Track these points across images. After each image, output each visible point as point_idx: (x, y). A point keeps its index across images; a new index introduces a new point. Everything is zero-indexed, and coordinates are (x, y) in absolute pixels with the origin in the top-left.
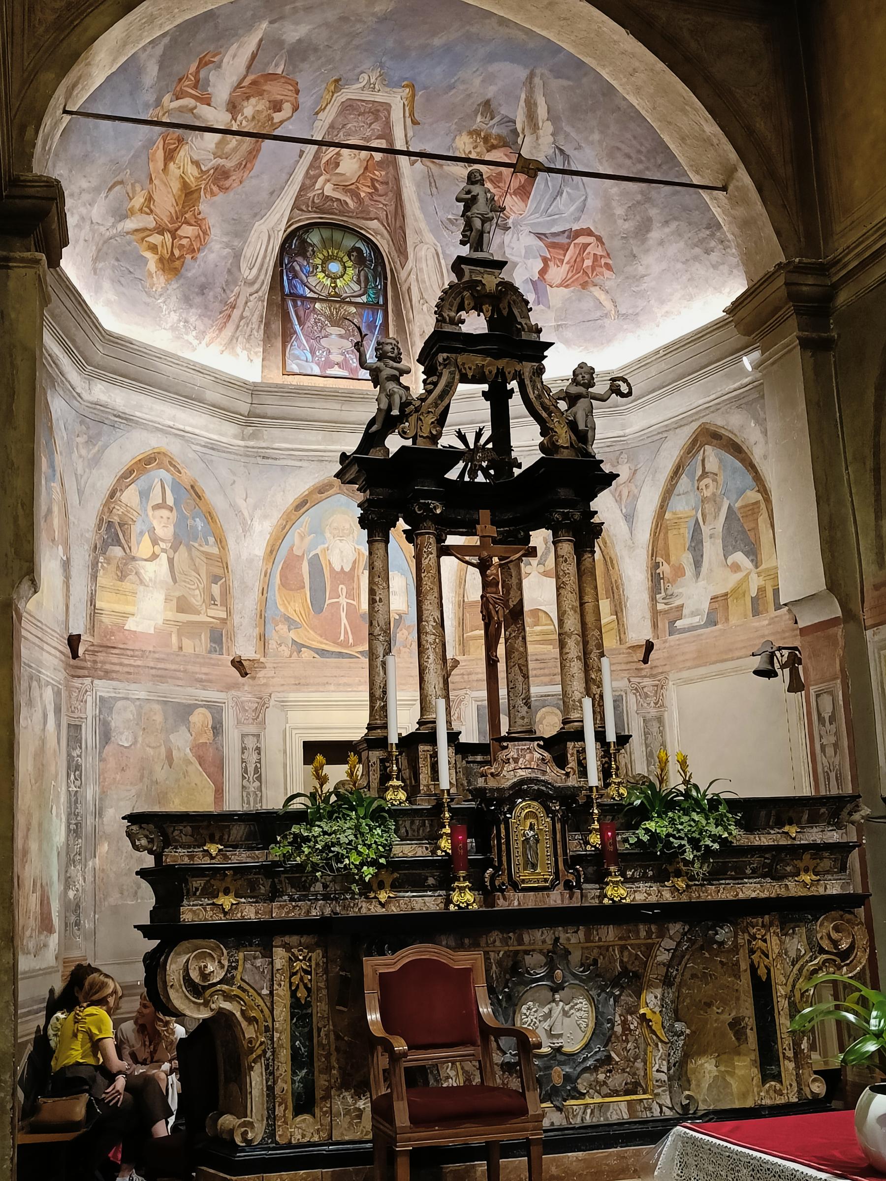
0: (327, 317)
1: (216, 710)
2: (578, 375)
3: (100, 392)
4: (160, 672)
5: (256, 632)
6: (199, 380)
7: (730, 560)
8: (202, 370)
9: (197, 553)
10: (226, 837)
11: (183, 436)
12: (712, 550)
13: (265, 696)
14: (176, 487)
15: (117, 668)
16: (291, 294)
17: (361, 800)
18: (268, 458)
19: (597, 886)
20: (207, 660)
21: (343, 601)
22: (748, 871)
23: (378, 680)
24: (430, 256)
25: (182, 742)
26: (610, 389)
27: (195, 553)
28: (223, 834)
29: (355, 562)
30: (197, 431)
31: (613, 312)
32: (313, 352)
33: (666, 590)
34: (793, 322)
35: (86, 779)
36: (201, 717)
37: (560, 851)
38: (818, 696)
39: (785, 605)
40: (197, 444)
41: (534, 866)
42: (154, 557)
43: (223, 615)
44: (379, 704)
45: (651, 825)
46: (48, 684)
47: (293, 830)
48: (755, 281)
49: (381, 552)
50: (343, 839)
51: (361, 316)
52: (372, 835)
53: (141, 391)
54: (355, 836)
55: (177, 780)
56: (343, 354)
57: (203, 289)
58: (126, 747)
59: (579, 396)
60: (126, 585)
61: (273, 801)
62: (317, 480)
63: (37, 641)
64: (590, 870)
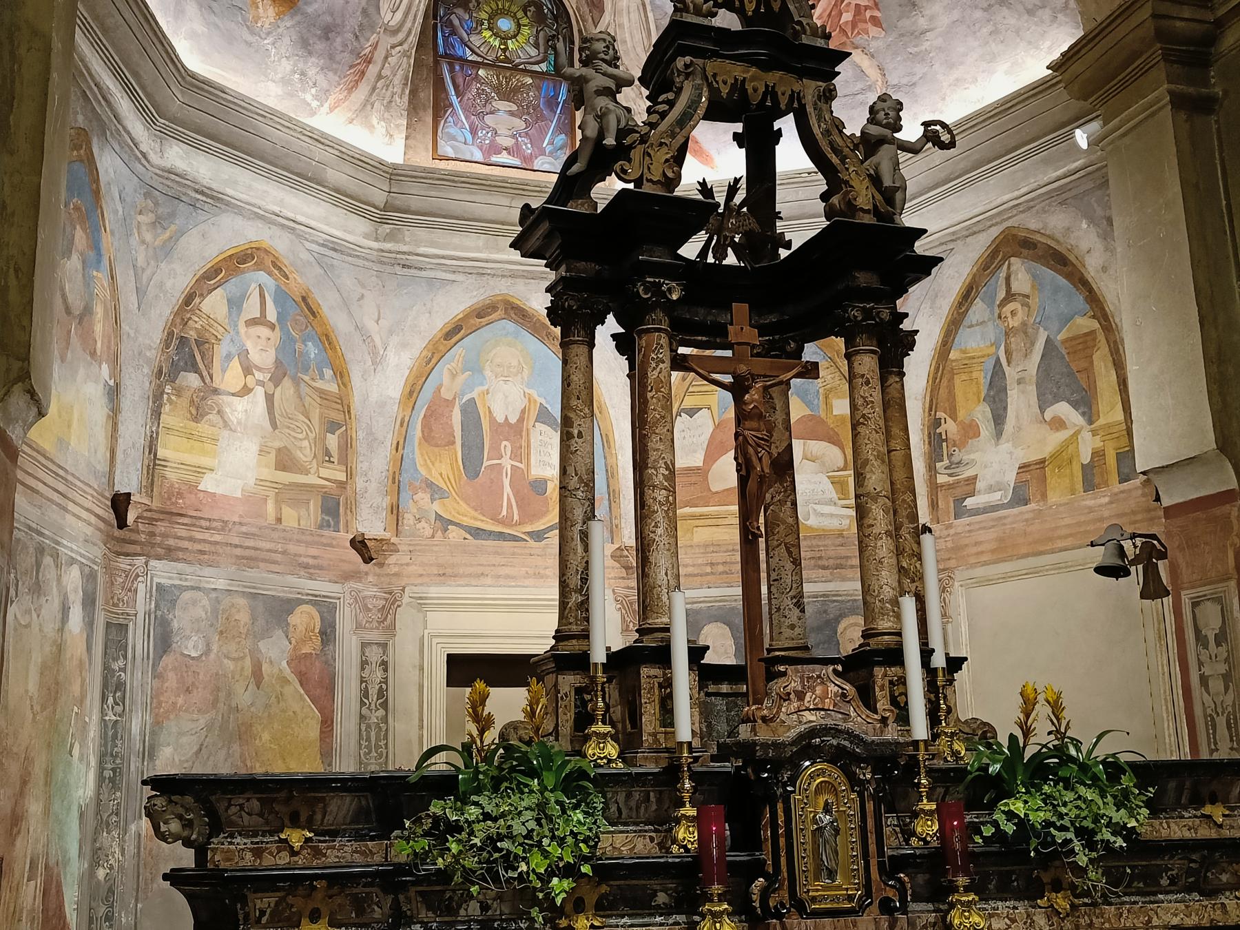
0: (494, 88)
1: (327, 609)
2: (877, 112)
3: (177, 156)
4: (248, 553)
5: (386, 502)
6: (318, 152)
7: (1049, 414)
8: (321, 139)
9: (307, 390)
10: (319, 817)
11: (293, 229)
12: (1021, 401)
13: (396, 590)
14: (282, 297)
15: (186, 544)
16: (446, 56)
17: (547, 757)
18: (409, 267)
19: (930, 906)
20: (317, 539)
21: (507, 463)
22: (1164, 882)
23: (575, 561)
24: (633, 7)
25: (276, 652)
26: (924, 135)
27: (304, 389)
28: (314, 812)
29: (523, 411)
30: (313, 223)
31: (880, 83)
32: (474, 132)
33: (950, 456)
34: (1160, 73)
35: (132, 703)
36: (304, 618)
37: (872, 848)
38: (1195, 605)
39: (1144, 473)
40: (313, 242)
41: (831, 874)
42: (246, 391)
43: (342, 477)
44: (575, 598)
45: (1018, 807)
46: (72, 561)
47: (432, 809)
48: (1099, 20)
49: (583, 360)
50: (518, 829)
51: (539, 89)
52: (567, 822)
53: (236, 161)
54: (538, 821)
55: (267, 706)
56: (513, 136)
57: (328, 32)
58: (193, 658)
59: (882, 141)
60: (203, 428)
61: (403, 760)
62: (475, 300)
63: (55, 497)
64: (921, 879)
